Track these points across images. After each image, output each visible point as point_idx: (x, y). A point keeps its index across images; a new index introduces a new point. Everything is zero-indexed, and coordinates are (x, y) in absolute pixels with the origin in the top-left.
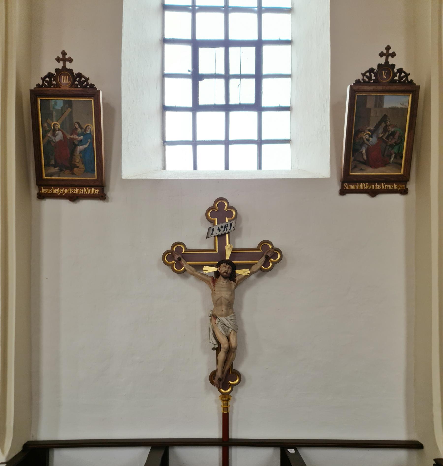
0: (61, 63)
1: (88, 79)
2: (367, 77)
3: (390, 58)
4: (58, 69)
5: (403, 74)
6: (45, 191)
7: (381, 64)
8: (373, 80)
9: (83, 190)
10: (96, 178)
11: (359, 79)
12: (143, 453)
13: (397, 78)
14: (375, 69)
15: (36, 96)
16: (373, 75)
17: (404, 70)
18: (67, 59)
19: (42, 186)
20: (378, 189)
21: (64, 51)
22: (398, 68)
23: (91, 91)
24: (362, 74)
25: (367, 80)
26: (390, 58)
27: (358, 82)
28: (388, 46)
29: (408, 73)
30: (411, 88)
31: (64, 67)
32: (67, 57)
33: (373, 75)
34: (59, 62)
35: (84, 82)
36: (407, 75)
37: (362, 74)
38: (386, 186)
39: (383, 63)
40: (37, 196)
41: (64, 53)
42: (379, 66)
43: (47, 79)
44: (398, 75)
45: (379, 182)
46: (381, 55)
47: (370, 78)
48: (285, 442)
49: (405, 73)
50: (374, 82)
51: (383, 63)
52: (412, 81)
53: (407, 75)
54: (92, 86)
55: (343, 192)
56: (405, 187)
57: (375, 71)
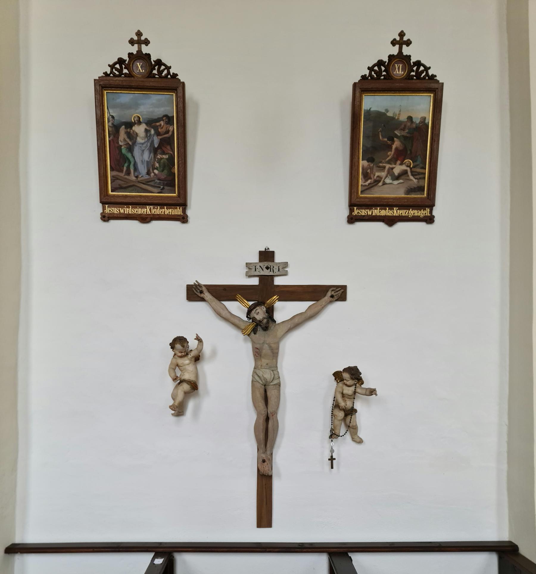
0: (136, 46)
1: (170, 67)
2: (376, 72)
3: (404, 47)
4: (132, 53)
5: (422, 68)
6: (358, 213)
7: (393, 55)
8: (384, 75)
9: (146, 210)
10: (425, 195)
11: (366, 75)
12: (145, 560)
13: (155, 72)
14: (126, 60)
15: (103, 87)
16: (383, 68)
17: (422, 62)
18: (405, 41)
19: (355, 206)
20: (364, 216)
21: (139, 31)
22: (414, 61)
23: (434, 85)
24: (369, 68)
25: (117, 73)
26: (404, 47)
27: (364, 77)
28: (402, 31)
29: (428, 66)
30: (173, 85)
31: (139, 51)
32: (143, 38)
33: (383, 68)
34: (133, 45)
35: (422, 72)
36: (427, 69)
37: (369, 68)
38: (398, 211)
39: (396, 54)
40: (347, 220)
41: (139, 34)
42: (391, 57)
43: (376, 68)
44: (156, 68)
45: (391, 207)
46: (394, 43)
47: (379, 73)
48: (122, 545)
49: (165, 65)
50: (384, 79)
51: (396, 54)
52: (433, 76)
53: (427, 69)
54: (175, 76)
55: (352, 220)
56: (431, 212)
57: (127, 62)
